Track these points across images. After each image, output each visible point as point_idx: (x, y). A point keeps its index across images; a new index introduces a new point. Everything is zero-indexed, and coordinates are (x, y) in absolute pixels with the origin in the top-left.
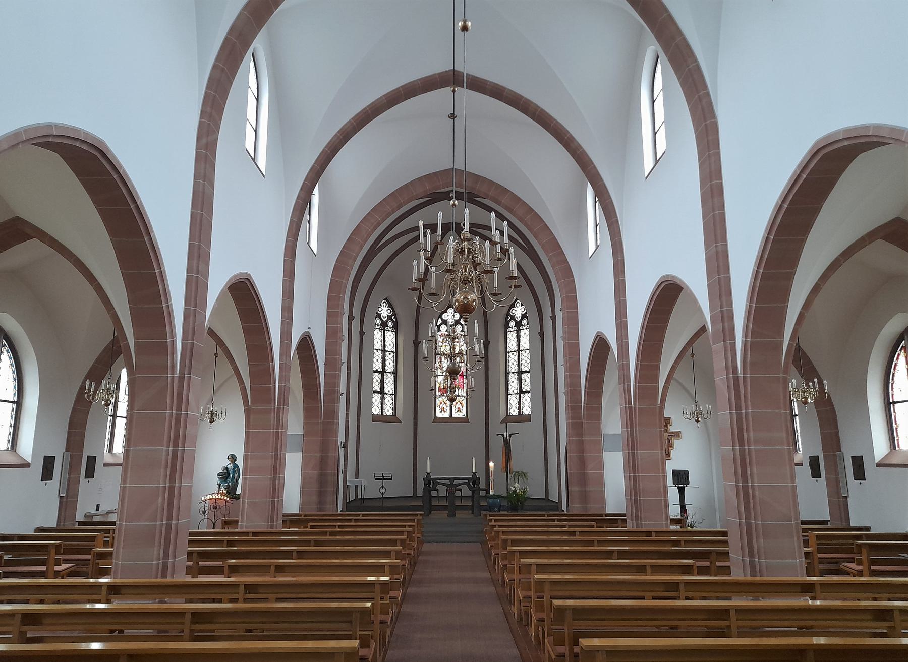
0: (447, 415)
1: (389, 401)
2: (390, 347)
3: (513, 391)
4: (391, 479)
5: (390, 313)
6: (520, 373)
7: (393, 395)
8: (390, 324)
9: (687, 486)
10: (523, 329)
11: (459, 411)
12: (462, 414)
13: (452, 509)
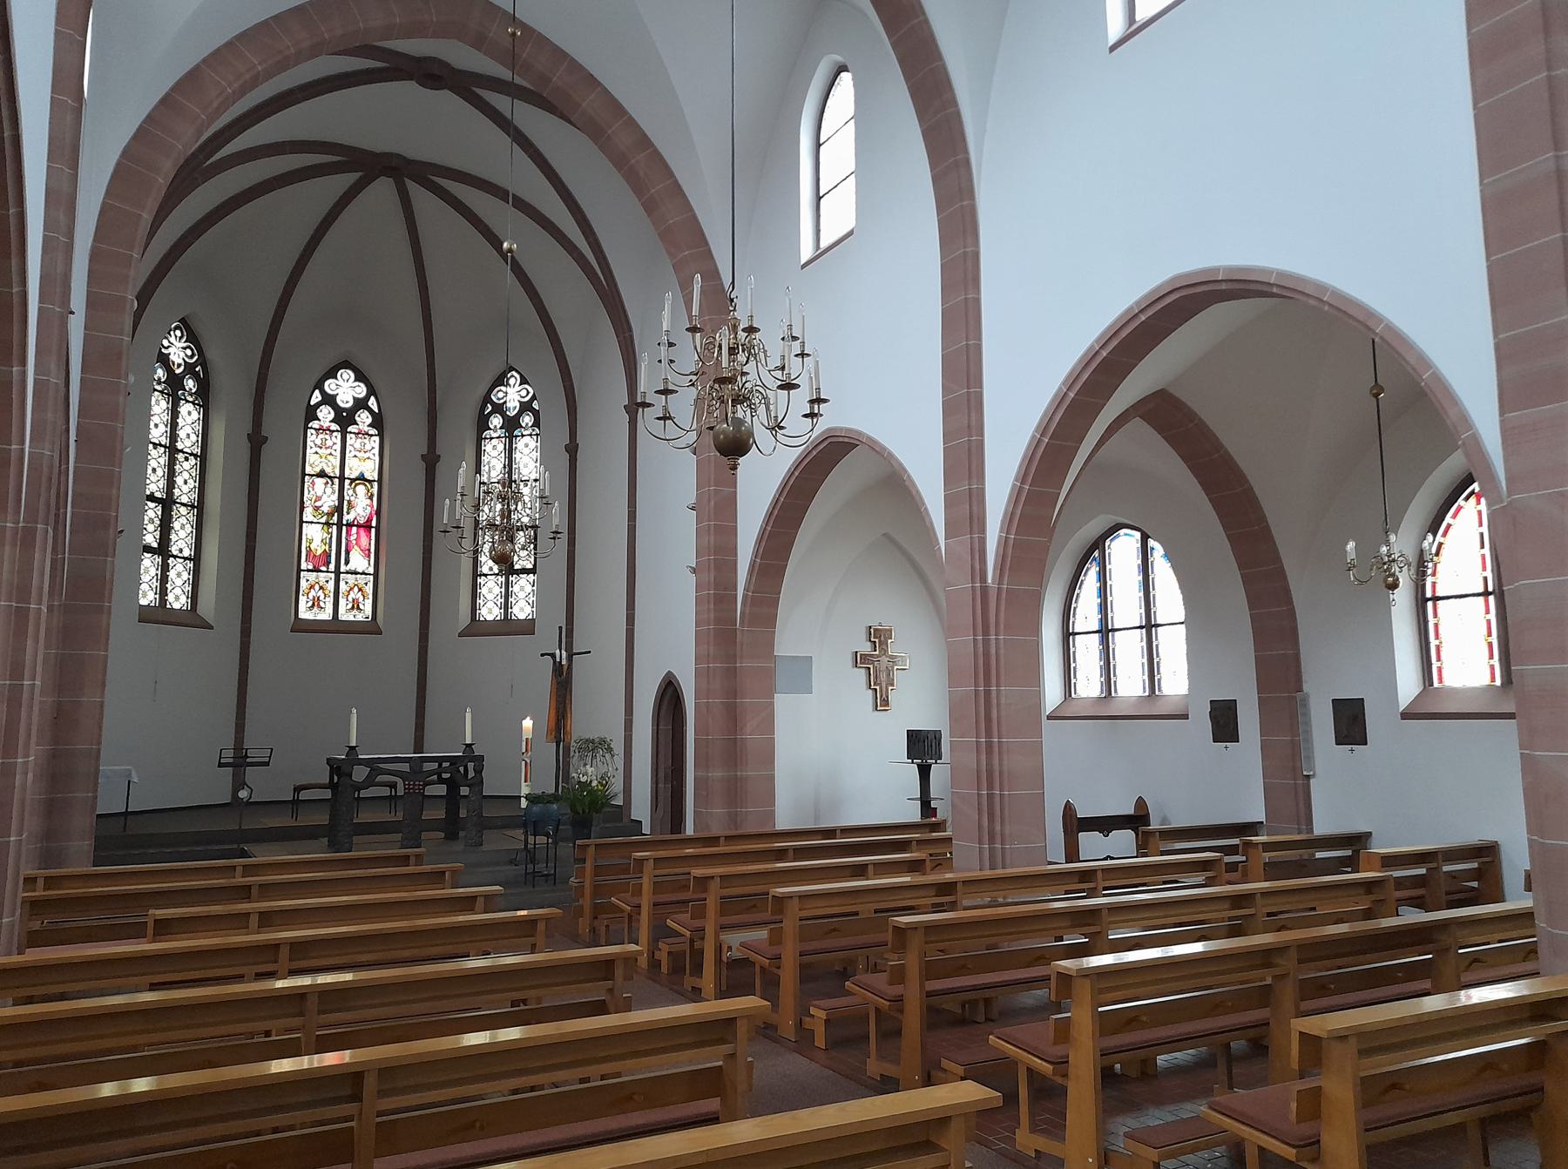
0: (326, 615)
1: (179, 574)
2: (188, 443)
5: (192, 357)
7: (190, 559)
8: (190, 384)
9: (936, 763)
10: (523, 436)
11: (356, 606)
13: (412, 831)
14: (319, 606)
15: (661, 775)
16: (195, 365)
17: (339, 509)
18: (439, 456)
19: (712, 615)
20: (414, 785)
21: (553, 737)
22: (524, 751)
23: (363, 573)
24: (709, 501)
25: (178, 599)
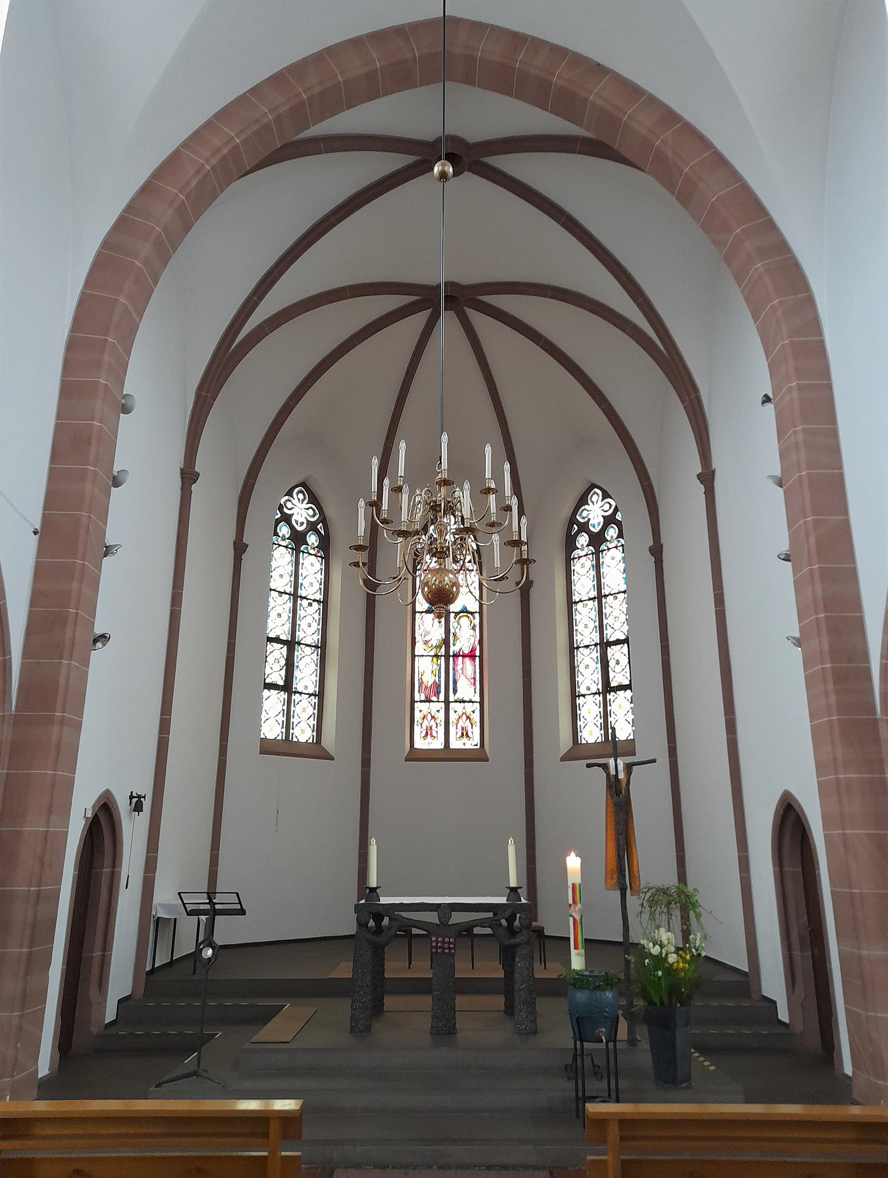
0: (438, 744)
1: (304, 709)
3: (588, 689)
4: (242, 912)
5: (314, 516)
6: (604, 645)
7: (315, 695)
8: (312, 539)
10: (609, 549)
11: (465, 734)
12: (472, 742)
14: (432, 735)
15: (795, 936)
16: (315, 524)
17: (446, 642)
18: (532, 581)
19: (833, 699)
20: (443, 942)
21: (614, 881)
22: (571, 901)
23: (470, 701)
24: (807, 536)
25: (303, 733)
